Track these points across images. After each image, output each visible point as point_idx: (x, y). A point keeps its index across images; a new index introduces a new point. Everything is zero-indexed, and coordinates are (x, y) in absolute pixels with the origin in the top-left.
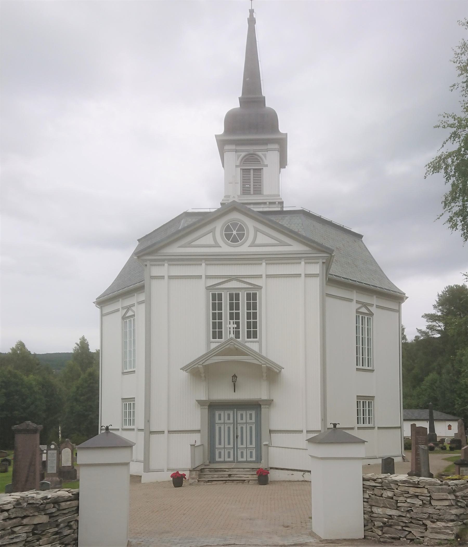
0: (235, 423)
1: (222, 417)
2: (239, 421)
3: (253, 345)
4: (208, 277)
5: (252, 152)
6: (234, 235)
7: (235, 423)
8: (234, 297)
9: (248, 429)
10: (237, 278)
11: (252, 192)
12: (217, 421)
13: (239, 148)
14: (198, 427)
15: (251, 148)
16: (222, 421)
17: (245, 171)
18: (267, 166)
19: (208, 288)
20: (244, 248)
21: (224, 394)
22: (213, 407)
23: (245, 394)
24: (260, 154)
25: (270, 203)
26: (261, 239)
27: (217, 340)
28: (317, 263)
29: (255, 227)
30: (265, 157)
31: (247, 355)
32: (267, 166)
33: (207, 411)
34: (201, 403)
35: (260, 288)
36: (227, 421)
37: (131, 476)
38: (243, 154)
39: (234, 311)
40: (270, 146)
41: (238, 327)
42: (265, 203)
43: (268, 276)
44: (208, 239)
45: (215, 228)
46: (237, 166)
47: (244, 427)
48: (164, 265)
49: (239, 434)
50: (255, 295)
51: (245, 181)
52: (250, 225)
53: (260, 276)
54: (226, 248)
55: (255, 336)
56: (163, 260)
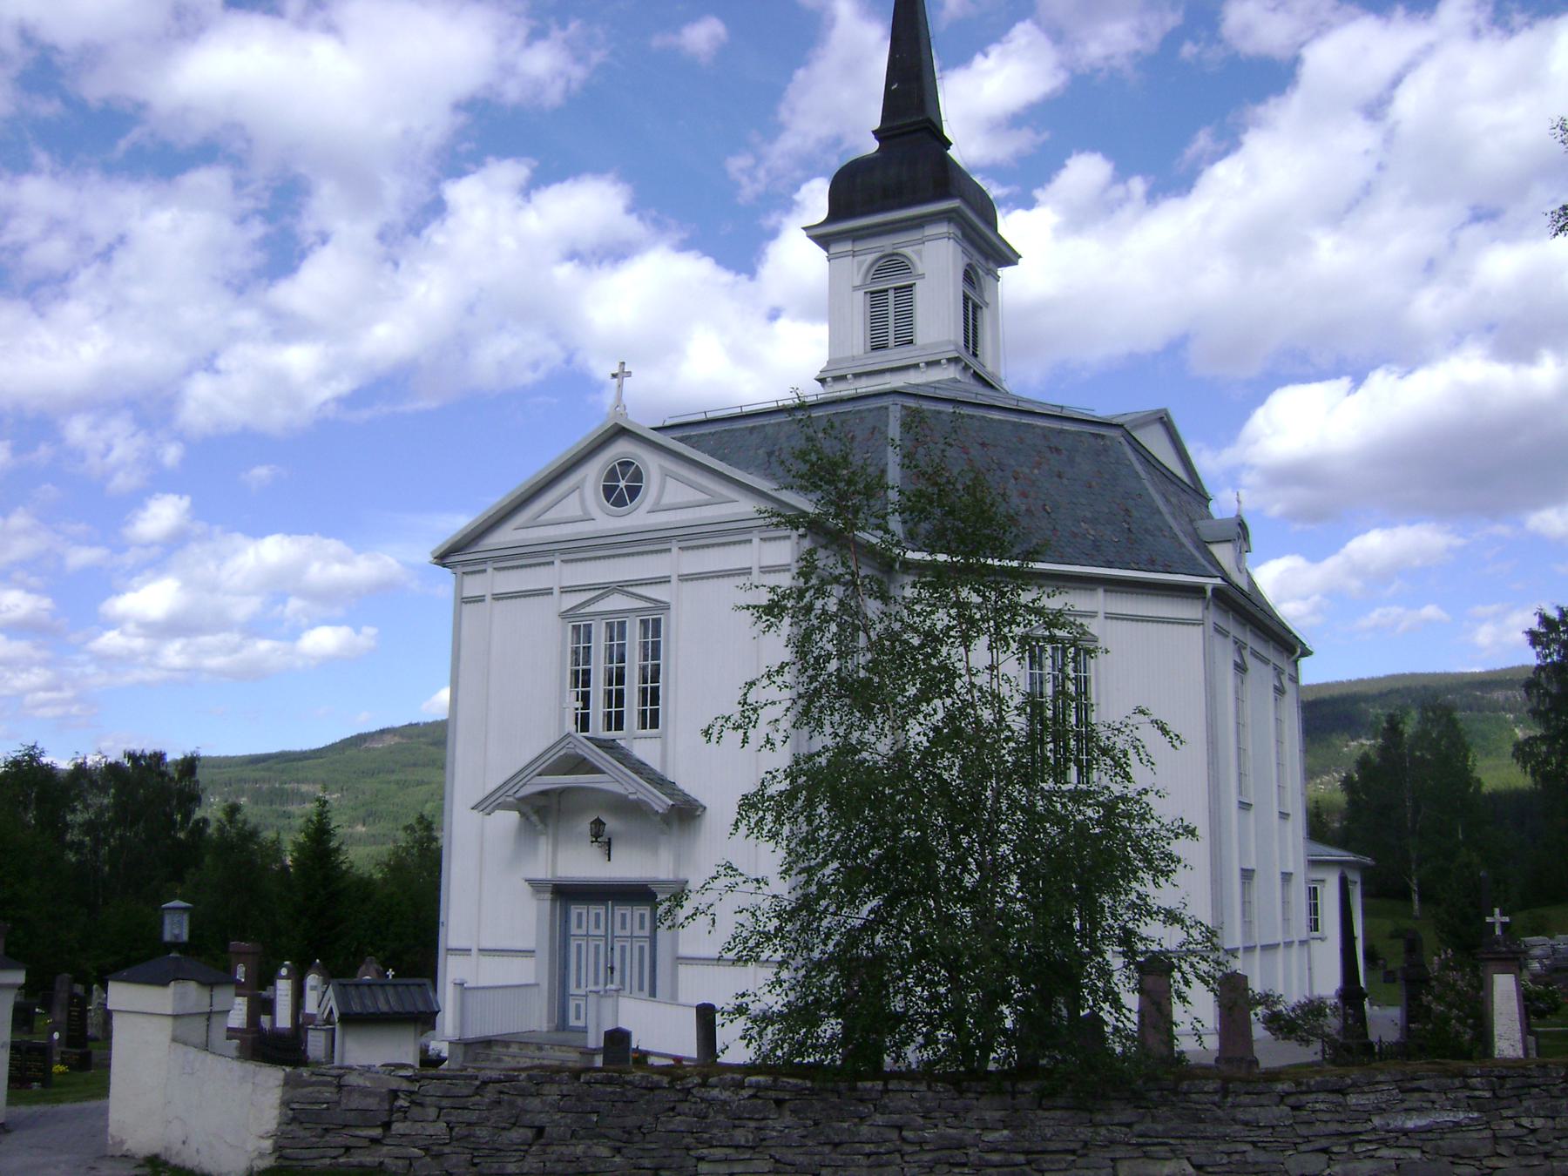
0: (609, 938)
1: (585, 916)
2: (618, 932)
3: (644, 748)
4: (566, 591)
5: (889, 250)
6: (622, 488)
7: (609, 938)
8: (617, 630)
9: (592, 949)
10: (620, 588)
11: (891, 343)
12: (574, 930)
13: (860, 246)
14: (529, 944)
15: (886, 244)
16: (583, 931)
17: (876, 296)
18: (922, 276)
19: (564, 615)
20: (638, 517)
21: (581, 863)
22: (567, 894)
23: (627, 866)
24: (907, 251)
25: (929, 364)
26: (676, 492)
27: (649, 731)
28: (788, 537)
29: (661, 467)
30: (920, 257)
31: (602, 772)
32: (922, 276)
33: (547, 904)
34: (536, 885)
35: (665, 607)
36: (593, 931)
37: (229, 1029)
38: (870, 258)
39: (581, 667)
40: (930, 231)
41: (586, 705)
42: (916, 366)
43: (684, 578)
44: (571, 507)
45: (584, 480)
46: (855, 288)
47: (628, 945)
48: (669, 550)
49: (617, 966)
50: (657, 622)
51: (876, 321)
52: (652, 464)
53: (665, 580)
54: (607, 521)
55: (655, 725)
56: (484, 561)
